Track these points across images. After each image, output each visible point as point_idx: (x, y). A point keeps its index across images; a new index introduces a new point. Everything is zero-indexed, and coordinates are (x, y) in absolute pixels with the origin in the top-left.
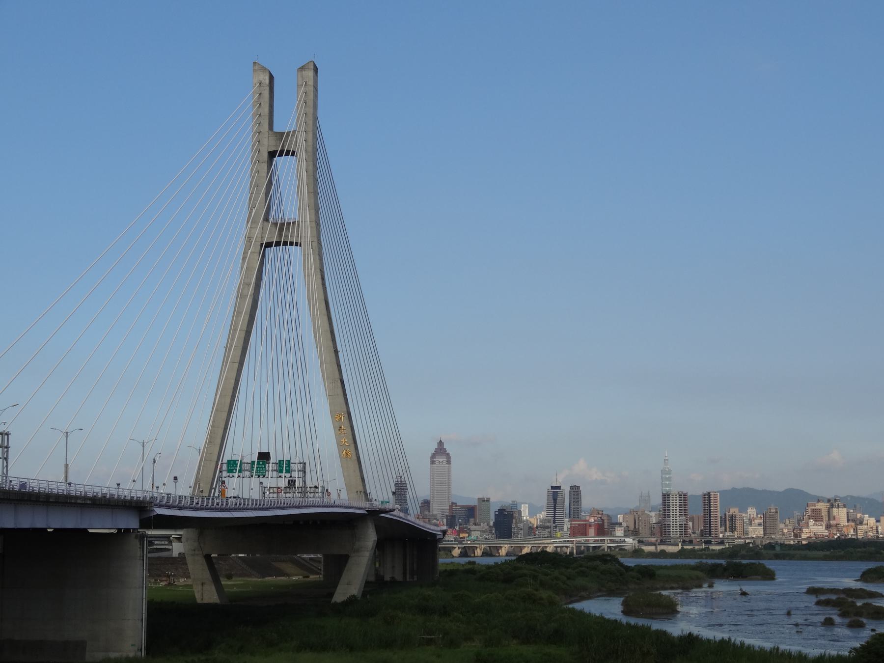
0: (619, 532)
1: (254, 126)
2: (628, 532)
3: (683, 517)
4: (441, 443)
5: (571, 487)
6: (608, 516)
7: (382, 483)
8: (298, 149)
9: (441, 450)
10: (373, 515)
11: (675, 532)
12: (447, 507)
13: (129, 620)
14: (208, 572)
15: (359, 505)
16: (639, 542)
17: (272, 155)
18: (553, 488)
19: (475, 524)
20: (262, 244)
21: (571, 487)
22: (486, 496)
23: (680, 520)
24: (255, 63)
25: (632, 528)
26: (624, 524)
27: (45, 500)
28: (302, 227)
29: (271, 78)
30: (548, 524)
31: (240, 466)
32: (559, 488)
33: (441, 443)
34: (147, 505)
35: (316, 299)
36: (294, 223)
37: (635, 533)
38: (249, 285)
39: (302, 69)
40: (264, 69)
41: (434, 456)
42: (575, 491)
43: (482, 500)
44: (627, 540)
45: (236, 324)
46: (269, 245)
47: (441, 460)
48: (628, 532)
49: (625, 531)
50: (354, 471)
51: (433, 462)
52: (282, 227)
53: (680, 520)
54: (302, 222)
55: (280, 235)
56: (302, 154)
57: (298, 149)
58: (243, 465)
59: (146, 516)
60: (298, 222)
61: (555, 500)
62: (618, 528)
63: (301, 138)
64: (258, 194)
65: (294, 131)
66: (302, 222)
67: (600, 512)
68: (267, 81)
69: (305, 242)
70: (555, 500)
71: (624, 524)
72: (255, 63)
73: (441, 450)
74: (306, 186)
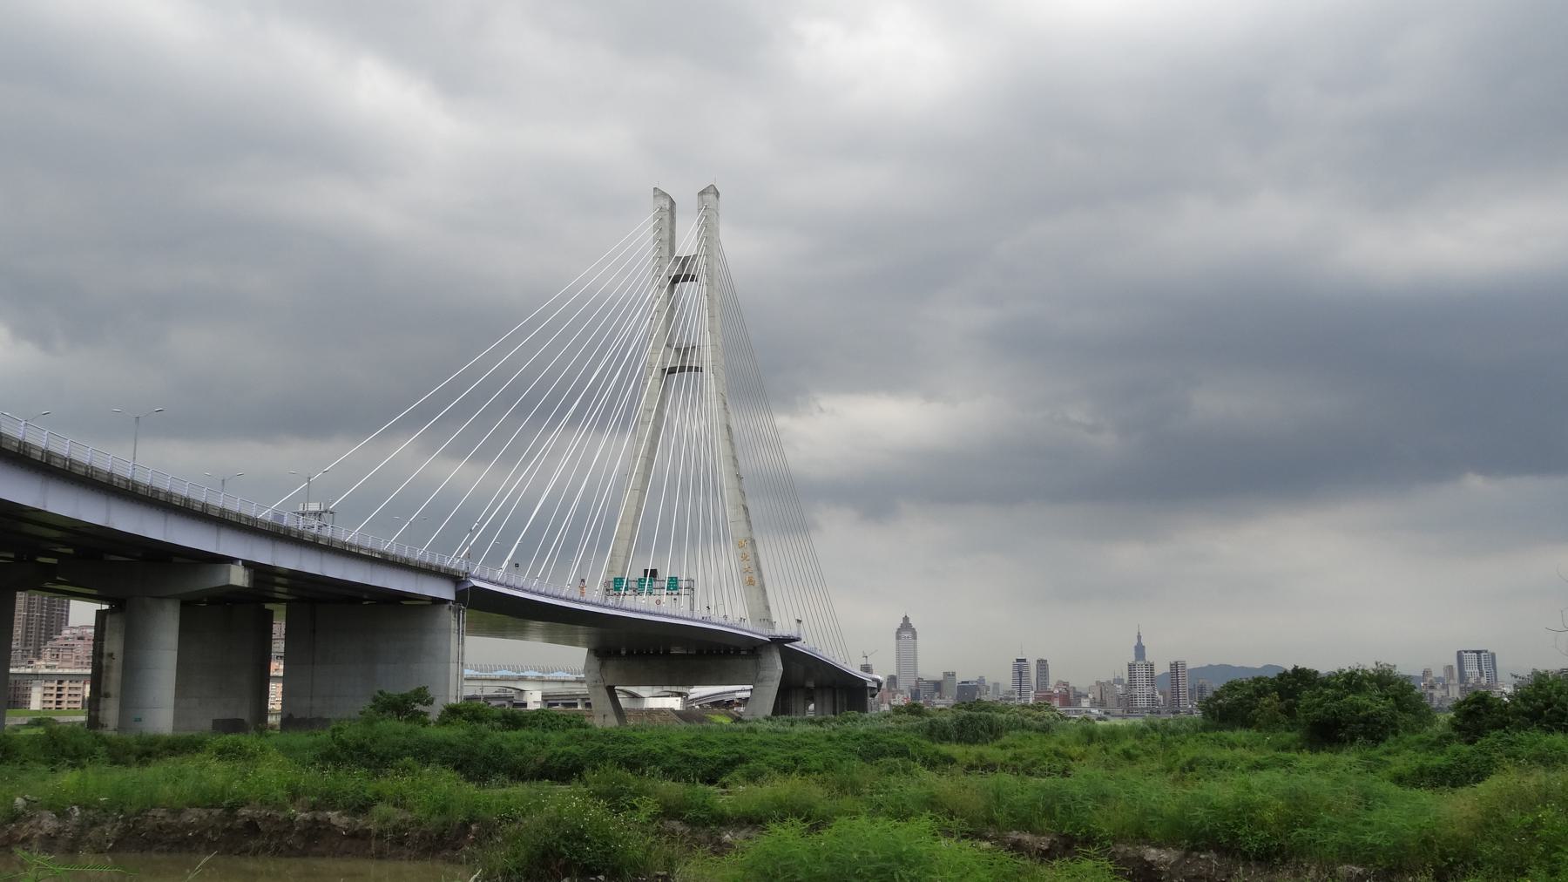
0: (1085, 703)
1: (654, 250)
2: (1093, 703)
3: (1150, 688)
4: (906, 619)
5: (1038, 661)
6: (1074, 688)
7: (820, 634)
8: (699, 273)
9: (906, 626)
10: (779, 642)
11: (1142, 703)
12: (913, 683)
13: (441, 696)
14: (610, 705)
15: (761, 633)
16: (1106, 713)
17: (675, 280)
18: (1018, 660)
19: (940, 697)
20: (664, 370)
21: (1038, 661)
22: (950, 670)
23: (1147, 690)
24: (655, 189)
25: (1098, 699)
26: (1091, 696)
27: (312, 540)
28: (703, 351)
29: (672, 203)
30: (1012, 696)
31: (627, 584)
32: (1024, 660)
33: (906, 619)
34: (461, 575)
35: (614, 345)
36: (694, 347)
37: (1101, 703)
38: (651, 410)
39: (702, 193)
40: (665, 195)
41: (899, 631)
42: (1042, 665)
43: (947, 674)
44: (1093, 711)
45: (637, 450)
46: (672, 371)
47: (906, 635)
48: (1093, 703)
49: (1091, 703)
50: (758, 599)
51: (898, 638)
52: (683, 351)
53: (1147, 690)
54: (703, 346)
55: (684, 360)
56: (703, 279)
57: (699, 273)
58: (629, 583)
59: (462, 587)
60: (699, 346)
61: (1020, 673)
62: (1083, 700)
63: (701, 261)
64: (659, 319)
65: (695, 256)
66: (703, 346)
67: (1066, 684)
68: (668, 207)
69: (706, 367)
70: (1020, 673)
71: (1091, 696)
72: (655, 189)
73: (906, 626)
74: (707, 311)
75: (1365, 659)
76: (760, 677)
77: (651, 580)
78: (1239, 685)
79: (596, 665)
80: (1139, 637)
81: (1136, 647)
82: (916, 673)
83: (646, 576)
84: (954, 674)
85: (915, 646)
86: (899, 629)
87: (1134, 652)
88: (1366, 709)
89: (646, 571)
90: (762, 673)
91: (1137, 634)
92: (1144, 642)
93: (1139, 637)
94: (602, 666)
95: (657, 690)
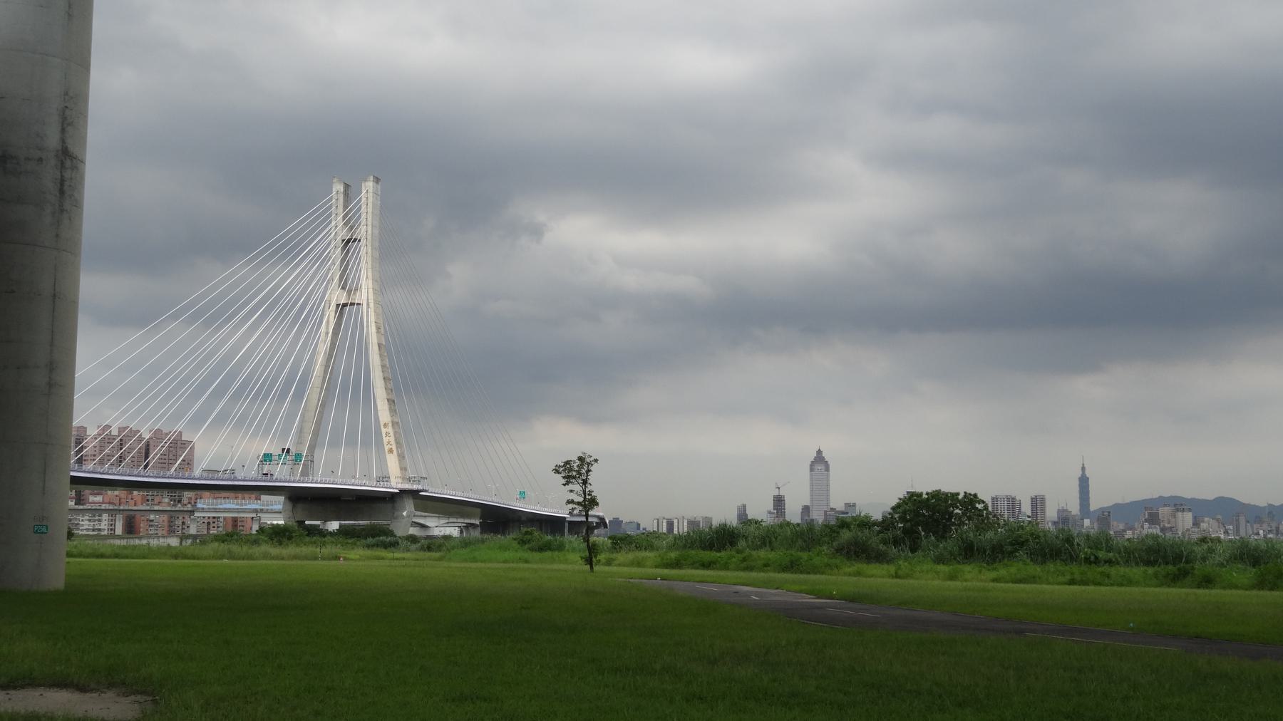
4: (819, 452)
9: (819, 459)
22: (851, 501)
33: (819, 452)
35: (280, 306)
43: (847, 505)
47: (820, 468)
51: (812, 470)
73: (819, 459)
75: (1114, 503)
76: (395, 515)
77: (286, 455)
78: (226, 540)
79: (289, 506)
80: (1083, 469)
81: (1080, 478)
82: (828, 504)
83: (283, 452)
84: (854, 505)
85: (828, 476)
86: (812, 462)
87: (1078, 483)
88: (1156, 575)
89: (283, 450)
90: (396, 514)
91: (1081, 466)
92: (1088, 474)
93: (1083, 469)
94: (294, 507)
95: (443, 521)
